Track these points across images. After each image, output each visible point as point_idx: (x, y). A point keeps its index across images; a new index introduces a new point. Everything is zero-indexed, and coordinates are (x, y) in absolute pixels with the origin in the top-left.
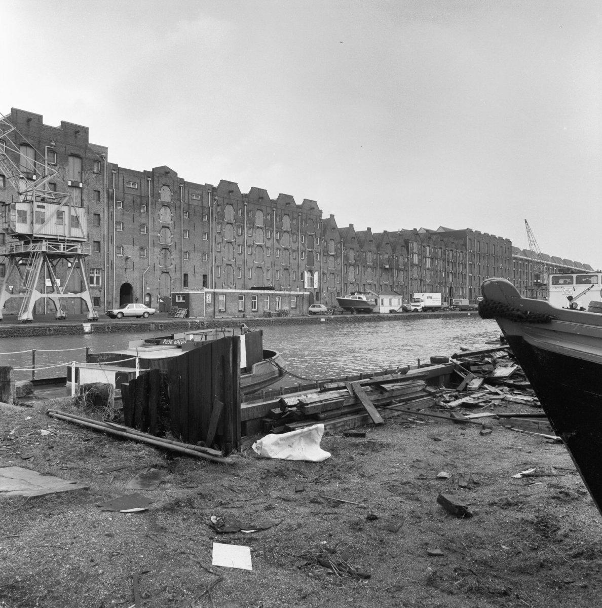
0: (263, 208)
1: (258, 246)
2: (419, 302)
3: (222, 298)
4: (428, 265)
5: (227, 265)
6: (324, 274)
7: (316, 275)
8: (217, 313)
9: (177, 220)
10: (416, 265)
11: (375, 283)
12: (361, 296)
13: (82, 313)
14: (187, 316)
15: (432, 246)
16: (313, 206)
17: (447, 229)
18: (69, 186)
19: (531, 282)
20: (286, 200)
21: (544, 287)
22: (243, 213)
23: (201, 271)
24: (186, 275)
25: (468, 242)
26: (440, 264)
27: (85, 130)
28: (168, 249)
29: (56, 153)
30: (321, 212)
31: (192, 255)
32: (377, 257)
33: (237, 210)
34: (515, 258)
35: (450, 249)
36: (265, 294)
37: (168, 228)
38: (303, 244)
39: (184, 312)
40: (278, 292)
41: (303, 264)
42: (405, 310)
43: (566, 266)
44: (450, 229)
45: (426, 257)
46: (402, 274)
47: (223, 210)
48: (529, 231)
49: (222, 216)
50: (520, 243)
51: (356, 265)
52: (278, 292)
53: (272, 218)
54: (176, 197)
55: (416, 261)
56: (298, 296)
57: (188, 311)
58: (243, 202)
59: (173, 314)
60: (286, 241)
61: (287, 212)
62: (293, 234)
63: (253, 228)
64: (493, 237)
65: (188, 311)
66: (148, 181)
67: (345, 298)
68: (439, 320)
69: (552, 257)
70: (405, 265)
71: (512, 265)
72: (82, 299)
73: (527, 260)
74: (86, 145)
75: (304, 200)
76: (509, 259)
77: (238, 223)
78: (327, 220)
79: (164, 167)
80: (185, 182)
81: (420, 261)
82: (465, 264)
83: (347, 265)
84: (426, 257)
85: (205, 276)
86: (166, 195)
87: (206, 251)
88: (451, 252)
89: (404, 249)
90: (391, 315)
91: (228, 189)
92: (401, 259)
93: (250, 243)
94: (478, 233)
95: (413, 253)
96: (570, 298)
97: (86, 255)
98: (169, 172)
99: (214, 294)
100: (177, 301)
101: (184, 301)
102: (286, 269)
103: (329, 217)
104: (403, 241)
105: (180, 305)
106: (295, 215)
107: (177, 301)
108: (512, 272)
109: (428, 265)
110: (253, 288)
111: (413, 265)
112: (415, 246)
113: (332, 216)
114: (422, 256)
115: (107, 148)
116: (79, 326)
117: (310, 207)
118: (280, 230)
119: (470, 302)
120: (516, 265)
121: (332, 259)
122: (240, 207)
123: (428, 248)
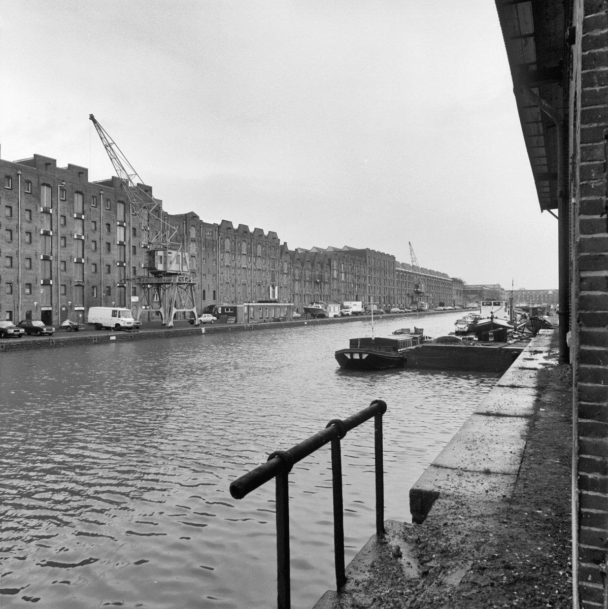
0: (246, 240)
1: (244, 268)
2: (348, 308)
3: (252, 309)
4: (343, 279)
5: (227, 283)
6: (281, 287)
7: (276, 288)
8: (250, 320)
9: (199, 251)
10: (335, 279)
11: (311, 294)
12: (319, 305)
13: (149, 320)
14: (236, 322)
15: (345, 263)
16: (275, 236)
17: (350, 247)
18: (75, 218)
19: (411, 289)
20: (259, 231)
21: (422, 294)
22: (235, 244)
23: (212, 288)
24: (204, 291)
25: (368, 258)
26: (350, 277)
27: (55, 161)
28: (194, 273)
29: (65, 190)
30: (279, 240)
31: (207, 276)
32: (312, 274)
33: (263, 246)
34: (398, 271)
35: (350, 263)
36: (272, 306)
37: (195, 257)
38: (269, 266)
39: (234, 319)
40: (278, 304)
41: (269, 280)
42: (343, 315)
43: (404, 270)
44: (353, 248)
45: (341, 272)
46: (327, 286)
47: (224, 242)
48: (412, 250)
49: (223, 246)
50: (402, 258)
51: (299, 281)
52: (278, 304)
53: (251, 247)
54: (198, 234)
55: (335, 276)
56: (288, 306)
57: (236, 319)
58: (235, 236)
59: (225, 321)
60: (260, 264)
61: (260, 241)
62: (263, 258)
63: (240, 255)
64: (383, 254)
65: (236, 319)
66: (183, 223)
67: (309, 307)
68: (360, 323)
69: (402, 263)
70: (329, 279)
71: (396, 276)
72: (192, 312)
73: (406, 272)
74: (150, 200)
75: (269, 232)
76: (394, 271)
77: (234, 252)
78: (283, 246)
79: (192, 213)
80: (203, 223)
81: (338, 275)
82: (366, 277)
83: (294, 280)
84: (341, 272)
85: (214, 292)
86: (193, 233)
87: (215, 273)
88: (357, 267)
89: (328, 266)
90: (334, 319)
91: (226, 225)
92: (326, 273)
93: (239, 266)
94: (374, 251)
95: (333, 270)
96: (492, 313)
97: (194, 284)
98: (196, 217)
99: (248, 307)
100: (226, 311)
101: (232, 312)
102: (259, 285)
103: (283, 244)
104: (327, 261)
105: (229, 315)
106: (264, 243)
107: (226, 311)
108: (396, 282)
109: (343, 279)
110: (260, 302)
111: (334, 279)
112: (335, 264)
113: (285, 243)
114: (339, 272)
115: (161, 201)
116: (199, 329)
117: (273, 236)
118: (256, 256)
119: (378, 307)
120: (398, 275)
121: (285, 276)
122: (233, 239)
123: (342, 265)
